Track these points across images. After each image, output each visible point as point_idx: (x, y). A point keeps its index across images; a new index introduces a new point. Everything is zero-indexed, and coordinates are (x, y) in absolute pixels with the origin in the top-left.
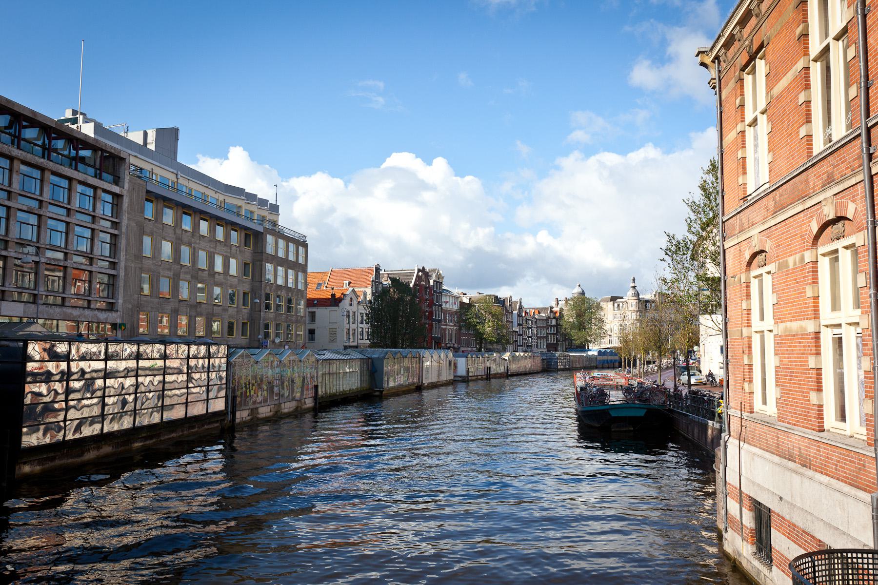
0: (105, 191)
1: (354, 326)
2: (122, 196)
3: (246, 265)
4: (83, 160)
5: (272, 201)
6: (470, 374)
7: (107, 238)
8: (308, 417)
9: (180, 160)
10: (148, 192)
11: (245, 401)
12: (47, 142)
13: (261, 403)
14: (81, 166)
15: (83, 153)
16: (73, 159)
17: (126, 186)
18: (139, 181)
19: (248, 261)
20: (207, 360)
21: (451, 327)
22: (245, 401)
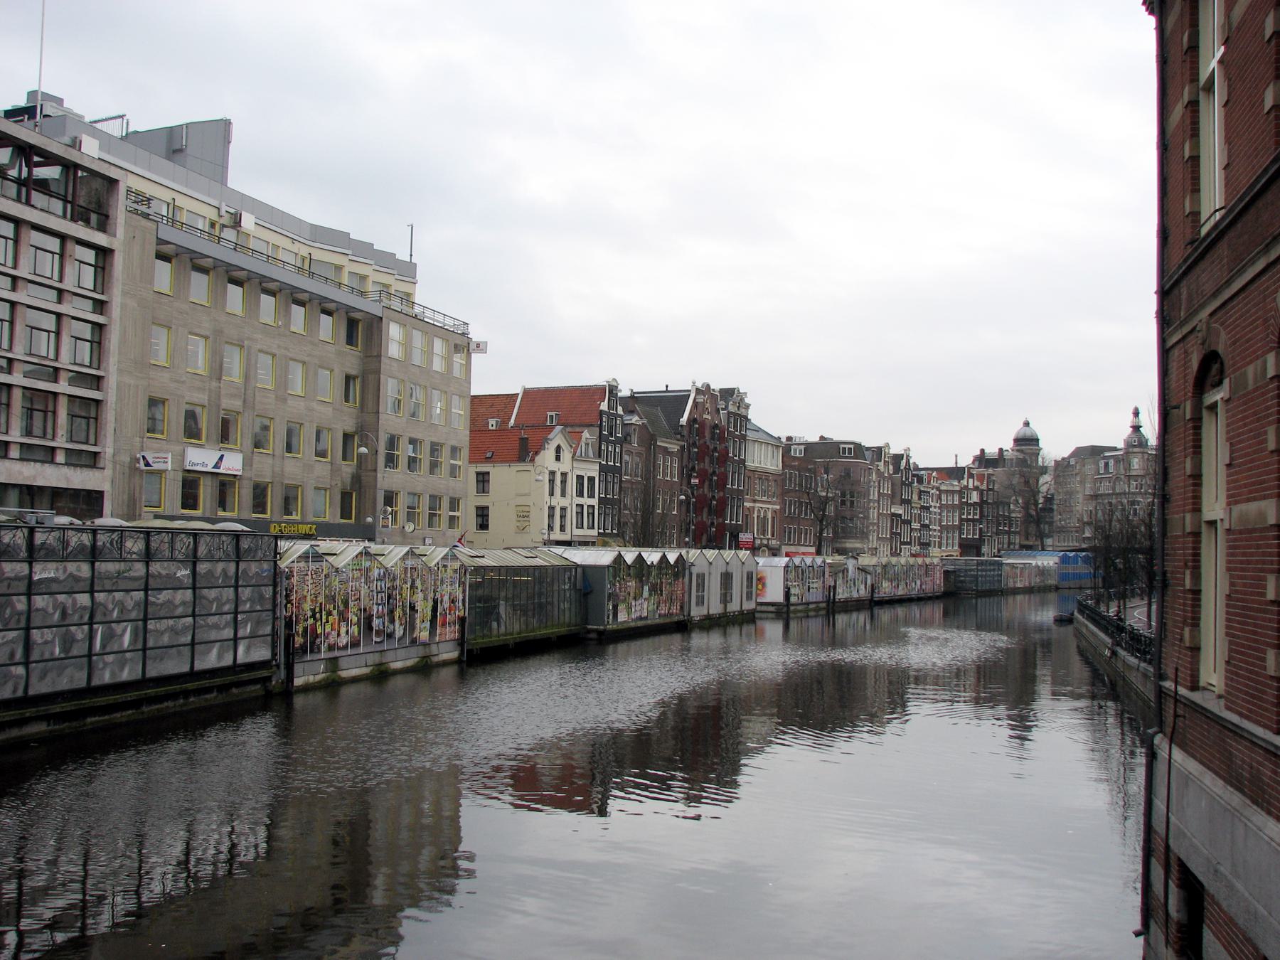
0: (81, 242)
1: (565, 502)
2: (112, 251)
3: (348, 379)
4: (43, 186)
5: (403, 256)
6: (793, 599)
7: (86, 331)
8: (448, 674)
9: (231, 184)
10: (161, 242)
11: (313, 643)
12: (25, 170)
13: (345, 647)
14: (37, 197)
15: (42, 172)
16: (20, 182)
17: (120, 232)
18: (144, 222)
19: (353, 372)
20: (232, 567)
21: (763, 507)
22: (313, 643)
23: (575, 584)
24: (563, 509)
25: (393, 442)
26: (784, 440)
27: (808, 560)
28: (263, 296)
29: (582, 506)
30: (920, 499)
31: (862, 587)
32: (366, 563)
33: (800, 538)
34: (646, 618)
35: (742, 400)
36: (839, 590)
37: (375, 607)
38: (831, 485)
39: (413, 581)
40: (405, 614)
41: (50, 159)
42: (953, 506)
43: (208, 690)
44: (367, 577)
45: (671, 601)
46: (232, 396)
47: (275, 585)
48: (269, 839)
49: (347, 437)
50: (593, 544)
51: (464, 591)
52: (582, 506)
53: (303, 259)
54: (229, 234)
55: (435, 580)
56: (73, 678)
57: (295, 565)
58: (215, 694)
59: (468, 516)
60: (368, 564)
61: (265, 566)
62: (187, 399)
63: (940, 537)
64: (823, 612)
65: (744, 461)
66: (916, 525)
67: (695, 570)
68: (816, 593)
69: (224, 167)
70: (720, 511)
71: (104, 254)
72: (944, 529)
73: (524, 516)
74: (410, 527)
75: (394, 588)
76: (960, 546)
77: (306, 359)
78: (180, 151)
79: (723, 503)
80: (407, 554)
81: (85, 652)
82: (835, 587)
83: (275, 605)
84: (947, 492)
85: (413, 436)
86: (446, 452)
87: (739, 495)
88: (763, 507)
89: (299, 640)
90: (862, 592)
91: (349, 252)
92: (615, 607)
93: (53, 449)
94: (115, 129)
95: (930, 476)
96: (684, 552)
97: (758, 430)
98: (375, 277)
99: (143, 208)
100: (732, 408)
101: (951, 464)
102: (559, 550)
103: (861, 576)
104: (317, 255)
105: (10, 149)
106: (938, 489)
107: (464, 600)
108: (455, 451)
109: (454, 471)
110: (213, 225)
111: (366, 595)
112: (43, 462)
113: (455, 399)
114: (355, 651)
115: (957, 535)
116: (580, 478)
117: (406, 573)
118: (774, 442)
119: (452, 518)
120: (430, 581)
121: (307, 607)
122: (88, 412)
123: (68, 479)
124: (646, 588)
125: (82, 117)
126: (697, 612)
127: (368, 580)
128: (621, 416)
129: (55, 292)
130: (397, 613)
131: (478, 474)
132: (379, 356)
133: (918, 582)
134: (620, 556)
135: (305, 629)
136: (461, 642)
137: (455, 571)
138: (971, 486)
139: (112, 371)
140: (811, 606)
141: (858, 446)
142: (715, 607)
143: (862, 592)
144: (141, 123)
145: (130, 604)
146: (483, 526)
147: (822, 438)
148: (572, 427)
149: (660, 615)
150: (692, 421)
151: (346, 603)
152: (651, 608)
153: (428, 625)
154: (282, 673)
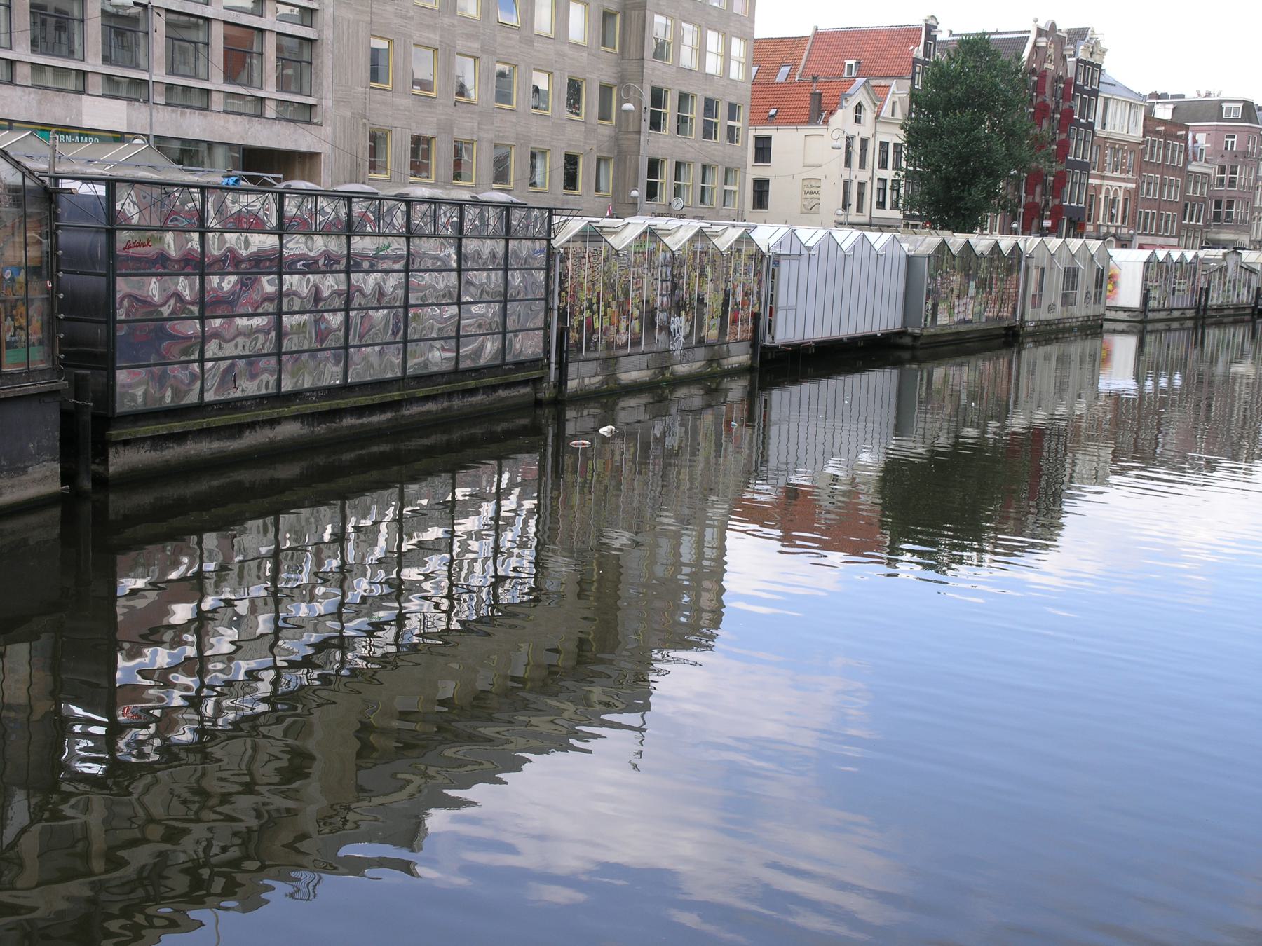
1: (864, 176)
3: (607, 16)
6: (1153, 304)
11: (589, 340)
13: (625, 346)
22: (589, 340)
24: (862, 185)
25: (658, 97)
29: (885, 180)
32: (649, 246)
33: (1158, 226)
34: (971, 321)
35: (1097, 42)
37: (659, 298)
39: (703, 268)
43: (473, 391)
44: (651, 262)
45: (1001, 300)
46: (469, 36)
48: (538, 563)
49: (605, 90)
51: (760, 282)
52: (885, 180)
55: (728, 268)
56: (331, 375)
57: (571, 245)
60: (653, 246)
64: (1190, 324)
67: (1033, 263)
68: (1182, 298)
75: (681, 276)
79: (1061, 179)
81: (341, 343)
82: (1208, 290)
85: (684, 89)
86: (723, 110)
88: (1113, 185)
89: (574, 336)
92: (935, 307)
93: (262, 100)
96: (1020, 239)
100: (1082, 55)
103: (1244, 277)
107: (759, 293)
114: (636, 350)
116: (884, 145)
117: (694, 258)
118: (1133, 101)
121: (584, 296)
122: (299, 57)
124: (973, 284)
126: (1033, 316)
134: (944, 243)
137: (750, 257)
140: (1176, 314)
149: (987, 318)
152: (977, 309)
153: (717, 321)
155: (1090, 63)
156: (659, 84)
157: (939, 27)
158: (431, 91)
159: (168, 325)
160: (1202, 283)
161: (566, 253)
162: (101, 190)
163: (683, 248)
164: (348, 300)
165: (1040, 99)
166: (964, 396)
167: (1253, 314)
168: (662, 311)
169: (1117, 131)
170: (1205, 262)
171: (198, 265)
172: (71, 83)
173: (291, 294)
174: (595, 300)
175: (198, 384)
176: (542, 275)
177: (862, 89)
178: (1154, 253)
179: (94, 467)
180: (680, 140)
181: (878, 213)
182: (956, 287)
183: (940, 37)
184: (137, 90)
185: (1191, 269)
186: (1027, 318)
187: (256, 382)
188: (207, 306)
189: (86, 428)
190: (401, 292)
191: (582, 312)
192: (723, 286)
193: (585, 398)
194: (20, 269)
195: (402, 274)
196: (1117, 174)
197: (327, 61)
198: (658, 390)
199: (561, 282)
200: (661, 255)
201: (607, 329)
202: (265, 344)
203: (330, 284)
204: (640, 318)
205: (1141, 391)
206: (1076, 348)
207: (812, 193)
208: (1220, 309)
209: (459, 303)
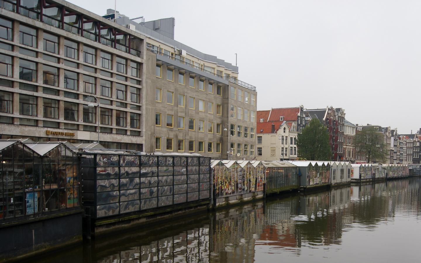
0: (132, 61)
1: (287, 146)
3: (218, 106)
4: (118, 41)
5: (234, 64)
6: (362, 178)
10: (158, 60)
11: (221, 192)
12: (97, 31)
13: (230, 194)
17: (145, 57)
18: (152, 54)
19: (220, 104)
21: (349, 147)
22: (221, 192)
23: (297, 172)
25: (232, 127)
26: (355, 125)
27: (363, 165)
28: (190, 78)
29: (292, 147)
30: (400, 145)
31: (384, 174)
32: (236, 166)
34: (318, 184)
35: (343, 112)
36: (376, 175)
37: (239, 180)
38: (371, 141)
39: (250, 172)
40: (248, 183)
41: (120, 32)
42: (411, 147)
44: (237, 171)
45: (325, 178)
46: (181, 112)
47: (210, 173)
49: (218, 125)
50: (296, 160)
51: (265, 175)
52: (292, 147)
53: (202, 66)
54: (178, 57)
55: (256, 172)
56: (153, 204)
58: (193, 209)
59: (255, 150)
60: (237, 166)
61: (207, 167)
62: (167, 113)
63: (406, 158)
65: (343, 132)
66: (398, 154)
67: (333, 168)
68: (369, 176)
69: (173, 34)
70: (336, 149)
71: (140, 64)
72: (408, 155)
73: (273, 150)
74: (239, 155)
75: (244, 174)
76: (413, 161)
77: (205, 99)
78: (158, 29)
79: (337, 146)
80: (248, 163)
82: (375, 174)
83: (210, 180)
84: (409, 143)
85: (239, 125)
86: (249, 130)
87: (342, 143)
88: (349, 147)
89: (217, 191)
90: (383, 176)
91: (224, 66)
92: (309, 180)
93: (126, 130)
94: (139, 21)
95: (403, 137)
96: (329, 162)
97: (348, 122)
98: (225, 72)
99: (151, 49)
100: (340, 115)
101: (410, 133)
102: (291, 162)
104: (206, 64)
105: (92, 23)
106: (406, 141)
107: (264, 178)
108: (252, 129)
109: (252, 136)
110: (172, 54)
111: (237, 177)
112: (123, 135)
113: (252, 112)
115: (412, 157)
117: (248, 169)
119: (252, 152)
120: (255, 172)
121: (219, 180)
122: (136, 119)
123: (132, 141)
124: (318, 174)
125: (129, 18)
127: (237, 172)
128: (304, 118)
129: (125, 78)
130: (245, 182)
131: (258, 137)
132: (228, 98)
133: (401, 172)
134: (316, 164)
135: (219, 188)
136: (264, 191)
137: (262, 169)
138: (417, 141)
139: (144, 103)
140: (368, 180)
141: (380, 127)
142: (338, 180)
143: (383, 175)
144: (148, 19)
145: (169, 180)
146: (260, 154)
147: (368, 125)
148: (289, 121)
150: (327, 119)
151: (230, 179)
152: (320, 180)
153: (254, 186)
154: (212, 202)
155: (342, 117)
156: (233, 123)
157: (304, 108)
158: (172, 126)
159: (111, 193)
160: (374, 172)
161: (215, 169)
162: (93, 157)
163: (245, 167)
164: (158, 183)
165: (330, 126)
166: (318, 204)
167: (386, 180)
168: (240, 184)
169: (349, 134)
170: (374, 167)
171: (118, 176)
172: (137, 134)
173: (144, 183)
174: (222, 181)
175: (118, 209)
176: (209, 175)
177: (285, 124)
178: (361, 165)
179: (91, 233)
180: (239, 138)
181: (291, 156)
182: (314, 175)
183: (304, 110)
184: (94, 129)
185: (370, 169)
186: (332, 182)
187: (134, 208)
188: (121, 186)
189: (89, 222)
190: (172, 182)
191: (219, 185)
192: (255, 176)
193: (221, 208)
194: (71, 177)
195: (172, 176)
196: (350, 145)
197: (144, 119)
198: (241, 204)
199: (214, 177)
200: (239, 169)
201: (226, 189)
202: (136, 197)
203: (154, 179)
204: (234, 186)
205: (360, 201)
206: (345, 191)
207: (273, 151)
208: (378, 178)
209: (187, 184)
